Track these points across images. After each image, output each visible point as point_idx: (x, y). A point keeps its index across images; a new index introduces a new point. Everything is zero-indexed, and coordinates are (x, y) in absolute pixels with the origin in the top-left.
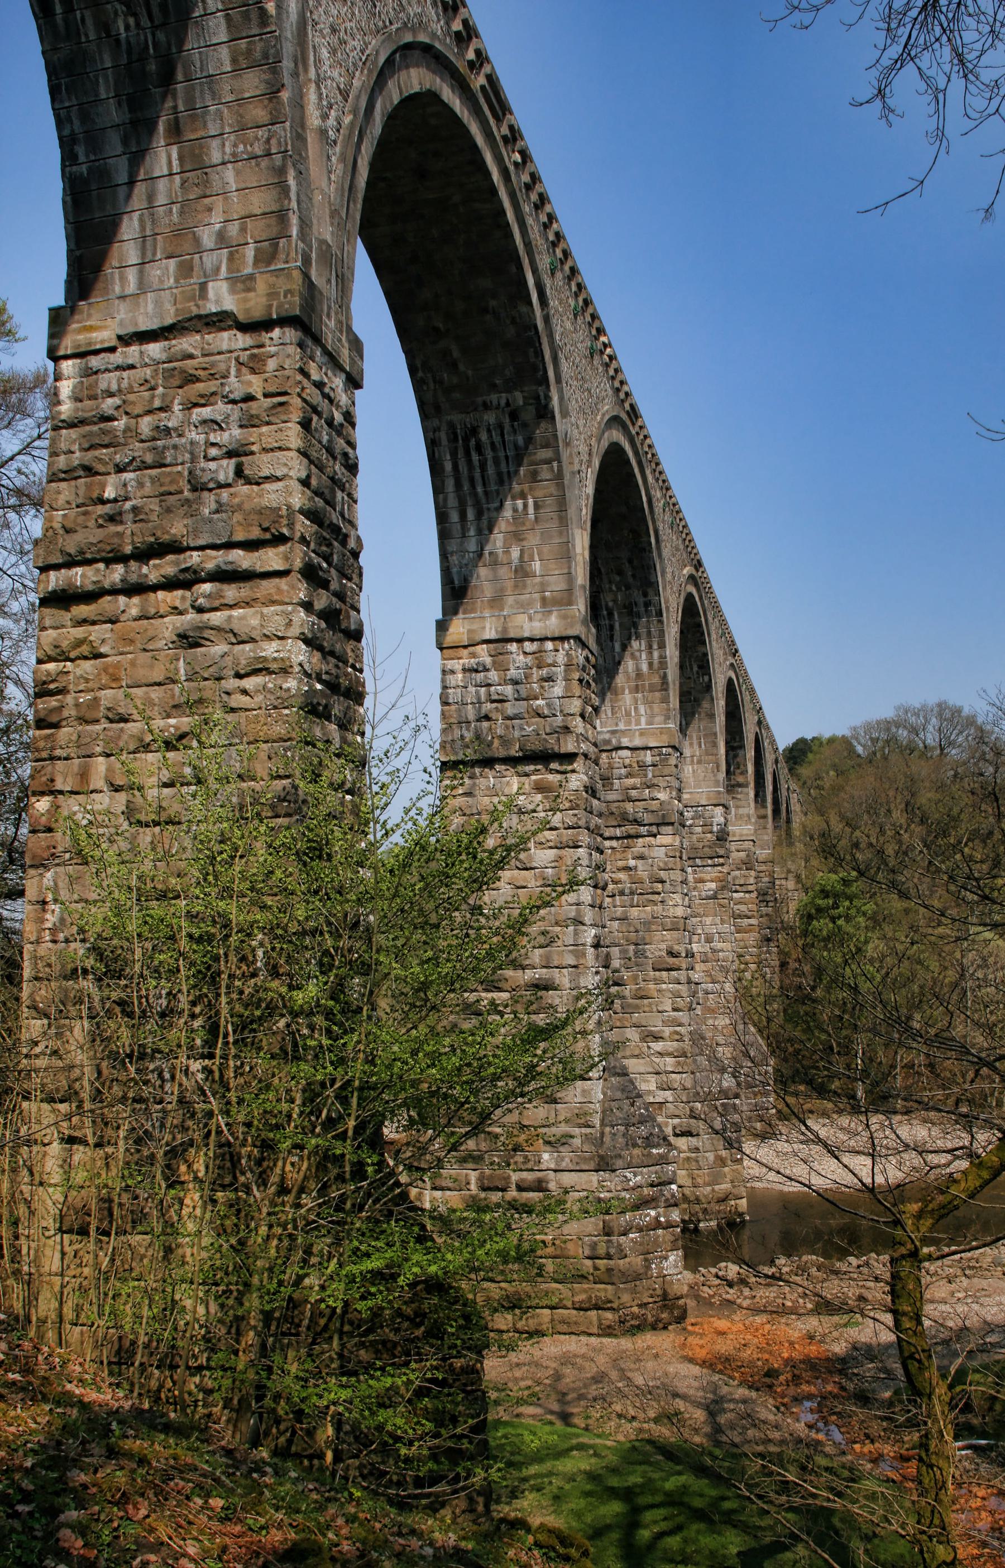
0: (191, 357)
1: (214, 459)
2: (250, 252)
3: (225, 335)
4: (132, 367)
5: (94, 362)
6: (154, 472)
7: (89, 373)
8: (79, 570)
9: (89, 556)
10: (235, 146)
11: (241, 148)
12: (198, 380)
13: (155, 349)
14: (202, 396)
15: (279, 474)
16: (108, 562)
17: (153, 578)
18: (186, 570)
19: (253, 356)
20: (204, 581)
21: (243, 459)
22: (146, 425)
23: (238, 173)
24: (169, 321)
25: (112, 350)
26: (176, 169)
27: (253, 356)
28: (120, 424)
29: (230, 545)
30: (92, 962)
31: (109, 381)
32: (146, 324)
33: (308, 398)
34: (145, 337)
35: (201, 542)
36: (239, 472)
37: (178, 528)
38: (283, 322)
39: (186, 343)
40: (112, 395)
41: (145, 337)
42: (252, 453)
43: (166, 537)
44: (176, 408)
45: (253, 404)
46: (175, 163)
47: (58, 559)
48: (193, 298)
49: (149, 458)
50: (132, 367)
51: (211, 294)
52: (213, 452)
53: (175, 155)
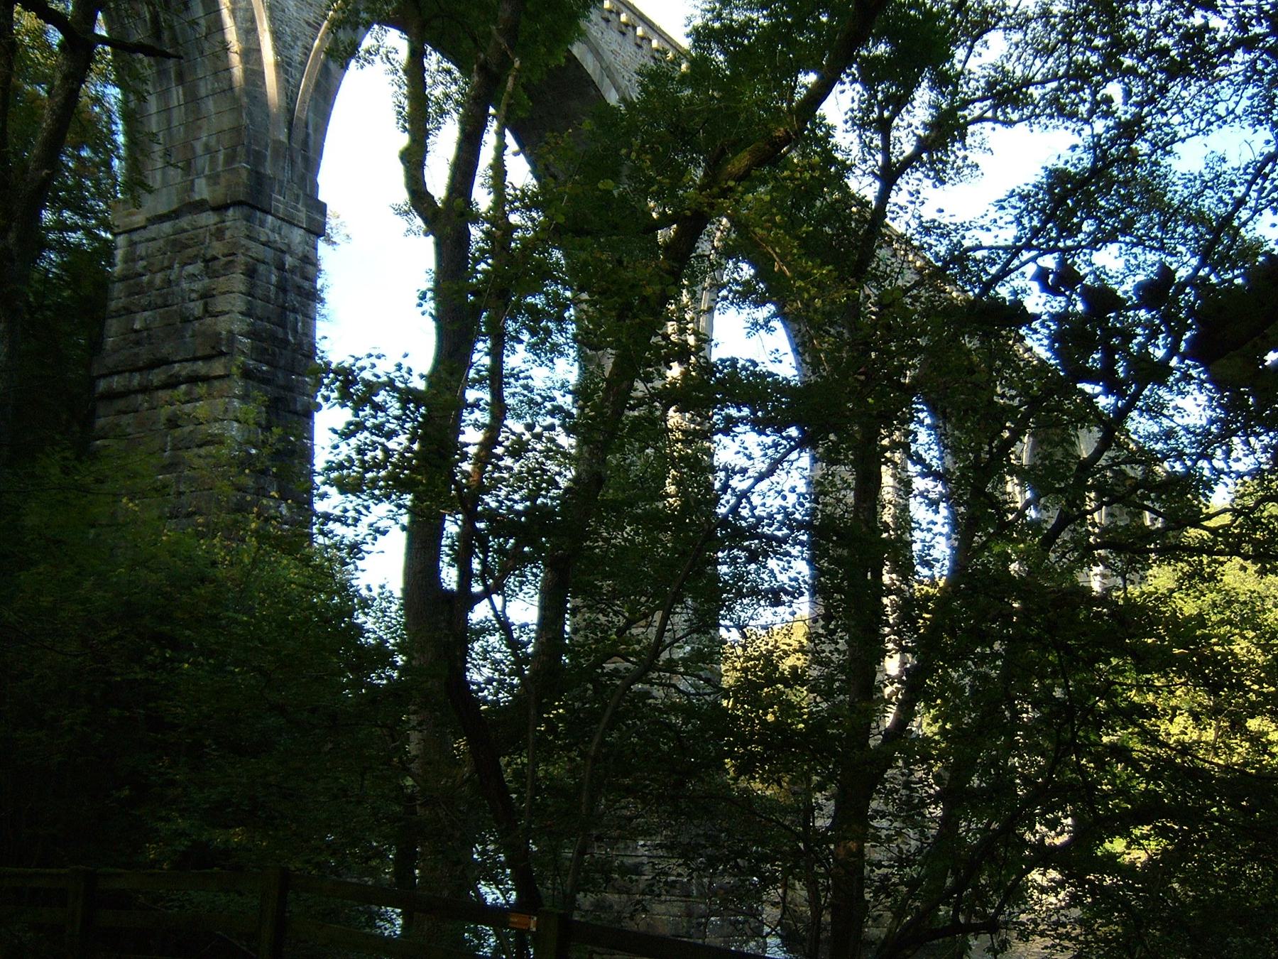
0: (185, 231)
1: (193, 300)
2: (221, 157)
3: (204, 215)
4: (154, 239)
5: (136, 237)
6: (161, 311)
7: (132, 244)
8: (116, 378)
9: (120, 369)
10: (213, 84)
11: (216, 85)
12: (188, 246)
13: (167, 227)
14: (189, 258)
15: (226, 309)
16: (131, 371)
17: (156, 382)
18: (171, 376)
19: (218, 229)
20: (182, 383)
21: (209, 300)
22: (159, 278)
23: (215, 102)
24: (175, 206)
25: (144, 227)
26: (182, 102)
27: (218, 229)
28: (145, 279)
29: (195, 359)
30: (1236, 649)
31: (141, 250)
32: (162, 210)
33: (253, 255)
34: (161, 219)
35: (179, 358)
36: (206, 311)
37: (166, 349)
38: (237, 204)
39: (184, 222)
40: (142, 259)
41: (161, 219)
42: (214, 296)
43: (158, 355)
44: (176, 266)
45: (216, 262)
46: (181, 97)
47: (105, 372)
48: (186, 191)
49: (159, 301)
50: (154, 239)
51: (196, 189)
52: (194, 296)
53: (181, 92)
